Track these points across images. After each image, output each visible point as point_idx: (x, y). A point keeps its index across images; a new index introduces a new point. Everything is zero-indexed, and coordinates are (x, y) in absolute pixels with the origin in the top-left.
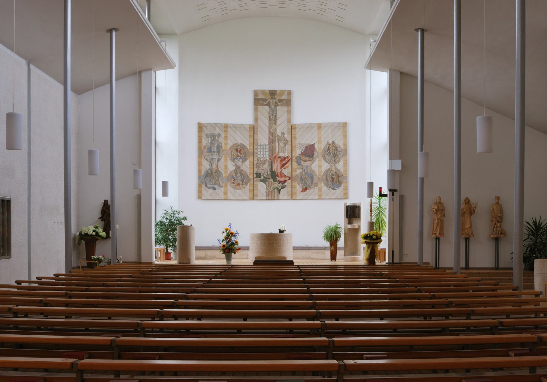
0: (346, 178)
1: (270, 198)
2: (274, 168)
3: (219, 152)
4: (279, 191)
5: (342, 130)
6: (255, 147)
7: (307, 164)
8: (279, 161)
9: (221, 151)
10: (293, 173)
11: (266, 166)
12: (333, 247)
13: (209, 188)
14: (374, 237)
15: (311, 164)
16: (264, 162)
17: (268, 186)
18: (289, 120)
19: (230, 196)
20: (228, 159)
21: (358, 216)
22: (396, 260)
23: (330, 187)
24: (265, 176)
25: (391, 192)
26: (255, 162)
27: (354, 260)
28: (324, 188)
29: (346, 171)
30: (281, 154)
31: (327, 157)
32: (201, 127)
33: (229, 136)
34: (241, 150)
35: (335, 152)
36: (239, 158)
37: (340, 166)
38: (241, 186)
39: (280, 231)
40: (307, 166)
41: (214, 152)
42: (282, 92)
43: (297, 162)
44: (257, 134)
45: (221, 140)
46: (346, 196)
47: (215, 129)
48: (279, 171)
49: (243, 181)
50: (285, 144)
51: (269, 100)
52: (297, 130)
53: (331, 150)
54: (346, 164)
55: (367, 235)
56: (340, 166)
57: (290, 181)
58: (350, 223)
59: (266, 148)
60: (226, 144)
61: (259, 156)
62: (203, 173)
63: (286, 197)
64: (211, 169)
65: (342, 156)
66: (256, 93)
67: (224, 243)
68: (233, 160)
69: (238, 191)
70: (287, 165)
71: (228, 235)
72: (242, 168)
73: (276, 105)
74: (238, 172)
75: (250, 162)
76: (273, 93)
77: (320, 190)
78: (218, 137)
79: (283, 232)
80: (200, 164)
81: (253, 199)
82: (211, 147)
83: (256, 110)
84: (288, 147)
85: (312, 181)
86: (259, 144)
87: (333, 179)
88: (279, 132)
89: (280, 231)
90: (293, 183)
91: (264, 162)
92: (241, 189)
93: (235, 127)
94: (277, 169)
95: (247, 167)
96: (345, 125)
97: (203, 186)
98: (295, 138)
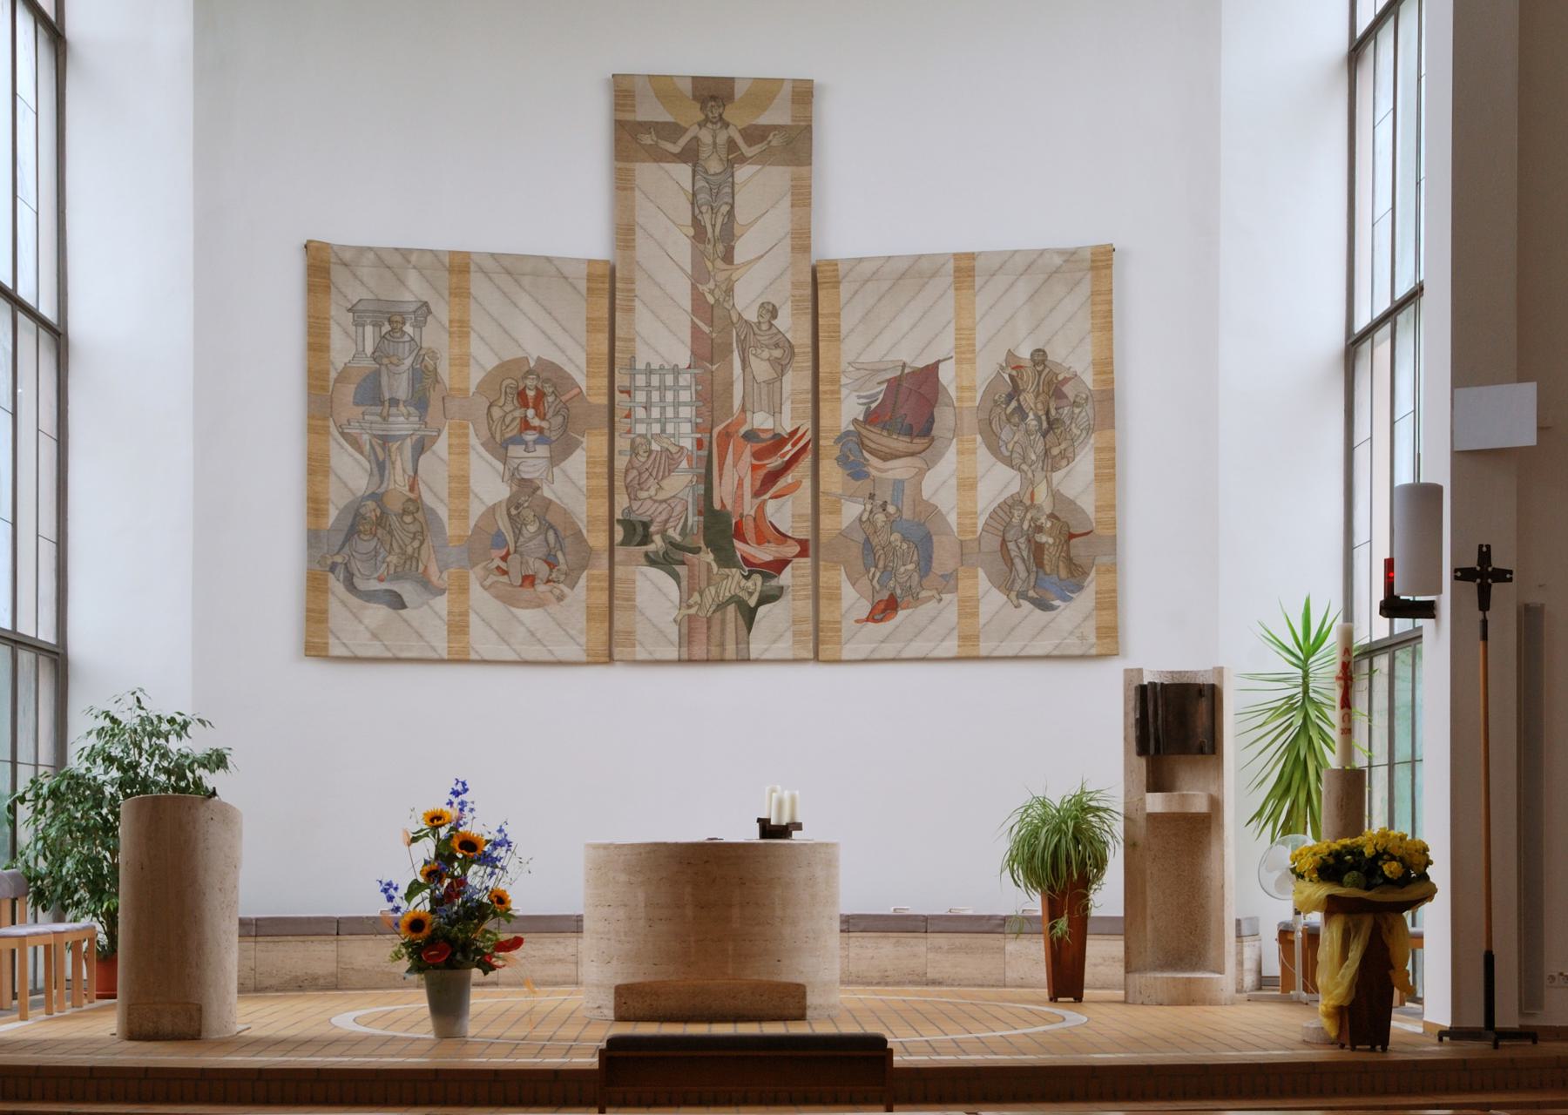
0: (1111, 544)
1: (699, 651)
2: (723, 494)
3: (420, 402)
4: (749, 616)
5: (1085, 289)
6: (621, 380)
7: (899, 469)
8: (747, 458)
9: (434, 398)
10: (826, 522)
11: (680, 484)
12: (1063, 924)
13: (370, 596)
14: (1391, 869)
15: (921, 474)
16: (669, 461)
17: (690, 589)
18: (801, 239)
19: (482, 640)
20: (474, 441)
21: (1209, 747)
22: (1508, 1017)
23: (1022, 595)
24: (674, 534)
25: (1472, 588)
26: (621, 463)
27: (1189, 997)
28: (992, 600)
29: (1113, 507)
30: (761, 421)
31: (1005, 434)
32: (321, 266)
33: (478, 321)
34: (540, 395)
35: (1051, 408)
36: (530, 436)
37: (1077, 480)
38: (541, 588)
39: (768, 830)
40: (898, 485)
41: (394, 402)
42: (765, 89)
43: (843, 460)
44: (631, 310)
45: (434, 336)
46: (1109, 640)
47: (402, 282)
48: (749, 507)
49: (551, 563)
50: (781, 367)
51: (693, 131)
52: (845, 290)
53: (1028, 399)
54: (1108, 472)
55: (1337, 855)
56: (1077, 480)
57: (806, 562)
58: (1158, 781)
59: (676, 388)
60: (463, 361)
61: (641, 429)
62: (333, 513)
63: (784, 648)
64: (377, 497)
65: (1089, 430)
66: (623, 91)
67: (422, 904)
68: (500, 448)
69: (526, 614)
70: (789, 479)
71: (445, 854)
72: (546, 492)
73: (733, 156)
74: (528, 514)
75: (591, 462)
76: (713, 94)
77: (969, 609)
78: (419, 325)
79: (783, 831)
80: (317, 467)
81: (610, 659)
82: (377, 374)
83: (623, 184)
84: (796, 381)
85: (925, 565)
86: (640, 365)
87: (1038, 550)
88: (746, 302)
89: (768, 830)
90: (824, 576)
91: (669, 461)
92: (540, 604)
93: (515, 270)
94: (738, 498)
95: (572, 484)
96: (1101, 261)
97: (336, 585)
98: (836, 336)
